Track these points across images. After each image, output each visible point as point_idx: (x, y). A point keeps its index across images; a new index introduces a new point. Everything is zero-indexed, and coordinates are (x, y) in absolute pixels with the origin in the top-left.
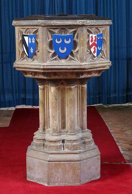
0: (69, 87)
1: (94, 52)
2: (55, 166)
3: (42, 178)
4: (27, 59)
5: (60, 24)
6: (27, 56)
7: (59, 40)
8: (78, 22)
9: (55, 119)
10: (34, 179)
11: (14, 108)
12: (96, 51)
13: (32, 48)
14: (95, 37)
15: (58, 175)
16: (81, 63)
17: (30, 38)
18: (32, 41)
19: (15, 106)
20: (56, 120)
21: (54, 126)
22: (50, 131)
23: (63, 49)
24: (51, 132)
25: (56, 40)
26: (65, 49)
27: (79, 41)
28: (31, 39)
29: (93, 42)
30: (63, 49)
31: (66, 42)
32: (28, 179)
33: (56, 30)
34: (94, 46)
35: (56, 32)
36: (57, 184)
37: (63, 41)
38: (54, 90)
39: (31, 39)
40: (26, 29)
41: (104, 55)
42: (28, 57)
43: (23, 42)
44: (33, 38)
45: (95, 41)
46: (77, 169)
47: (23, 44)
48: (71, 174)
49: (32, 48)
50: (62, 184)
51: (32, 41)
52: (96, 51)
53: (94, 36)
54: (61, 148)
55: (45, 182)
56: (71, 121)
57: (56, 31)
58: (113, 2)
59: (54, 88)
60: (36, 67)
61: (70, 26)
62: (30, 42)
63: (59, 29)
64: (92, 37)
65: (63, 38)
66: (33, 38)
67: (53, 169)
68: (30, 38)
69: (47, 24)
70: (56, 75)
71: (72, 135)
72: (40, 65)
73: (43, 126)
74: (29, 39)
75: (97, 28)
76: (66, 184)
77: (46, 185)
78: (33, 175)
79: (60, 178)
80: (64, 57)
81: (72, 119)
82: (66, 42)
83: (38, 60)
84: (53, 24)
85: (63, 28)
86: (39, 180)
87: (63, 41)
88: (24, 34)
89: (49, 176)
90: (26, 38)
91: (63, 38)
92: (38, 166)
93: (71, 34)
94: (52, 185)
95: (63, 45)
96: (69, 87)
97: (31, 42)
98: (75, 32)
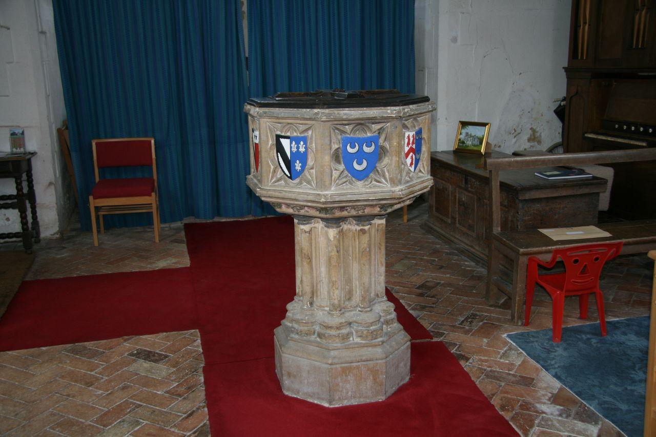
0: (362, 227)
1: (411, 164)
2: (343, 372)
3: (318, 394)
4: (285, 181)
5: (357, 116)
6: (287, 176)
7: (353, 147)
8: (389, 111)
9: (337, 287)
10: (298, 393)
11: (180, 222)
12: (414, 163)
13: (298, 162)
14: (413, 136)
15: (348, 386)
16: (393, 187)
17: (294, 143)
18: (298, 148)
19: (181, 219)
20: (337, 289)
21: (335, 299)
22: (324, 307)
23: (360, 163)
24: (327, 309)
25: (348, 147)
26: (365, 164)
27: (390, 148)
28: (298, 143)
29: (410, 146)
30: (360, 163)
31: (366, 149)
32: (286, 393)
33: (347, 127)
34: (411, 154)
35: (349, 131)
36: (346, 403)
37: (361, 148)
38: (335, 235)
39: (298, 143)
40: (284, 124)
41: (424, 167)
42: (290, 178)
43: (280, 149)
44: (302, 143)
45: (413, 143)
46: (379, 373)
47: (277, 152)
48: (369, 383)
49: (298, 162)
50: (354, 402)
51: (298, 148)
52: (414, 163)
53: (412, 134)
54: (349, 338)
55: (323, 399)
56: (364, 288)
57: (348, 128)
58: (317, 4)
59: (334, 231)
60: (310, 198)
61: (374, 120)
62: (294, 150)
63: (354, 125)
64: (409, 137)
65: (361, 142)
66: (302, 143)
67: (339, 377)
68: (294, 143)
69: (332, 117)
70: (343, 211)
71: (366, 312)
72: (319, 195)
73: (311, 297)
74: (291, 143)
75: (415, 119)
76: (362, 400)
77: (326, 405)
78: (296, 386)
79: (352, 392)
80: (361, 176)
81: (366, 284)
82: (366, 149)
83: (311, 185)
84: (345, 117)
85: (361, 124)
86: (310, 396)
87: (361, 148)
88: (279, 133)
89: (332, 390)
90: (285, 143)
91: (361, 142)
92: (309, 371)
93: (374, 134)
94: (337, 405)
95: (360, 156)
96: (362, 227)
97: (304, 150)
98: (380, 131)
